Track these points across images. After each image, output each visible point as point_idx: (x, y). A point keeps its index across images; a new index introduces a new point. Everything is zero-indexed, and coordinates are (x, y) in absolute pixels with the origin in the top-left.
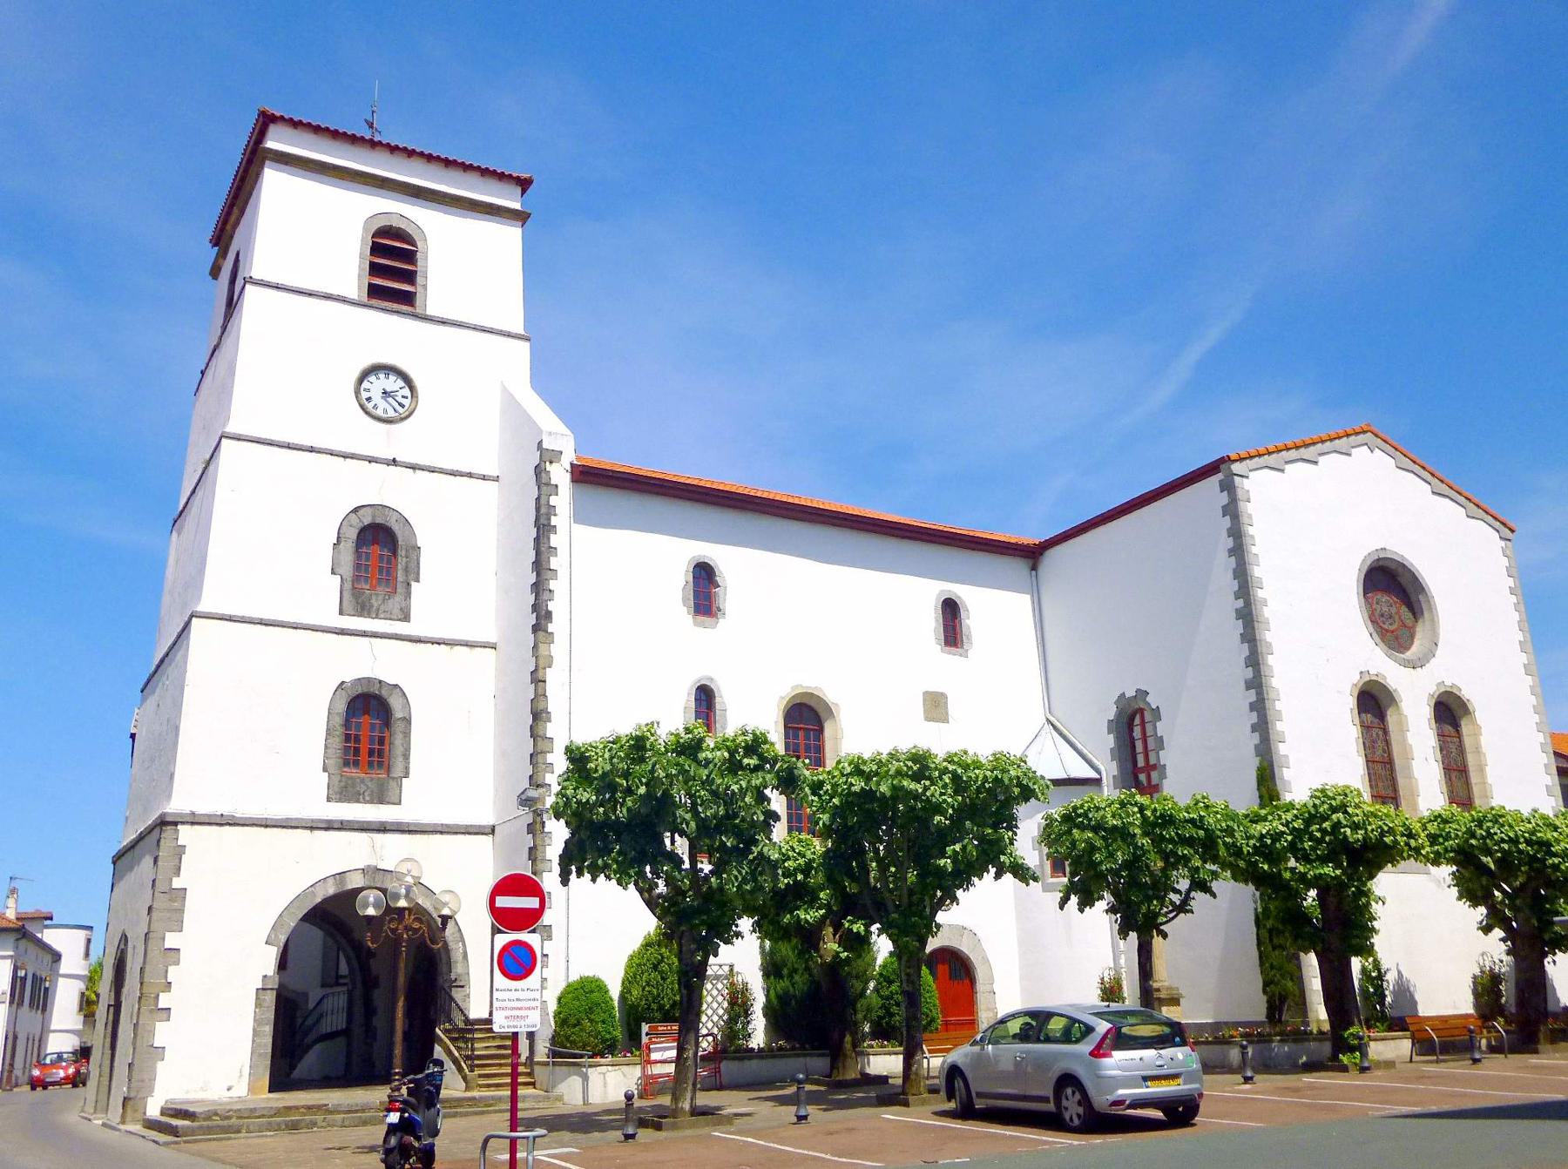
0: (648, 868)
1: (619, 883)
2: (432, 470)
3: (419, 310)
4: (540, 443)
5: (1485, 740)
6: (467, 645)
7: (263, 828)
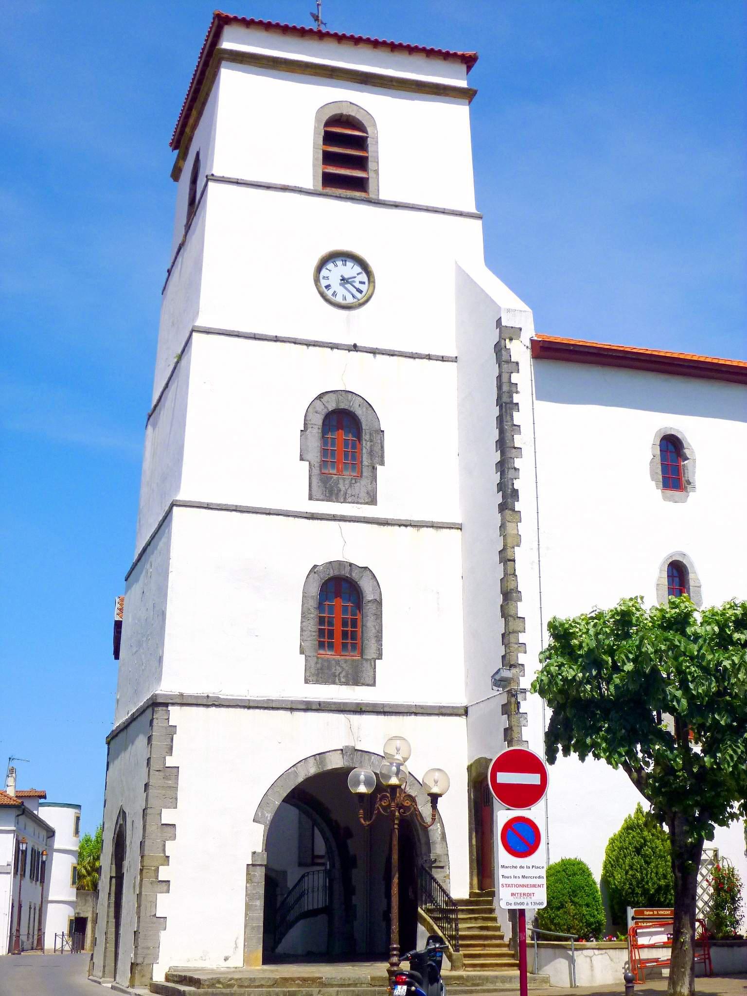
0: (639, 747)
1: (609, 763)
2: (392, 354)
3: (372, 196)
4: (499, 321)
6: (432, 527)
7: (246, 709)
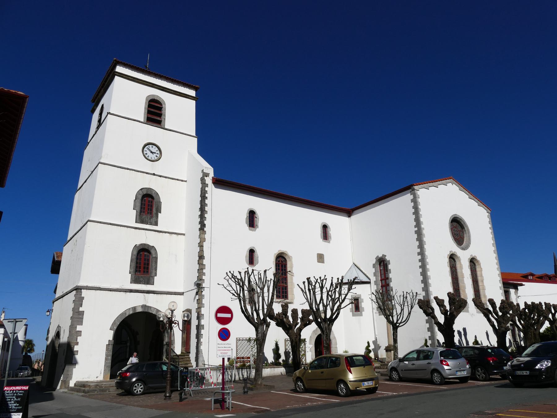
3: (163, 126)
5: (484, 273)
